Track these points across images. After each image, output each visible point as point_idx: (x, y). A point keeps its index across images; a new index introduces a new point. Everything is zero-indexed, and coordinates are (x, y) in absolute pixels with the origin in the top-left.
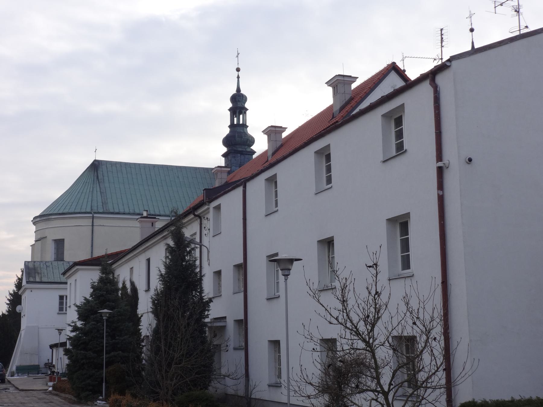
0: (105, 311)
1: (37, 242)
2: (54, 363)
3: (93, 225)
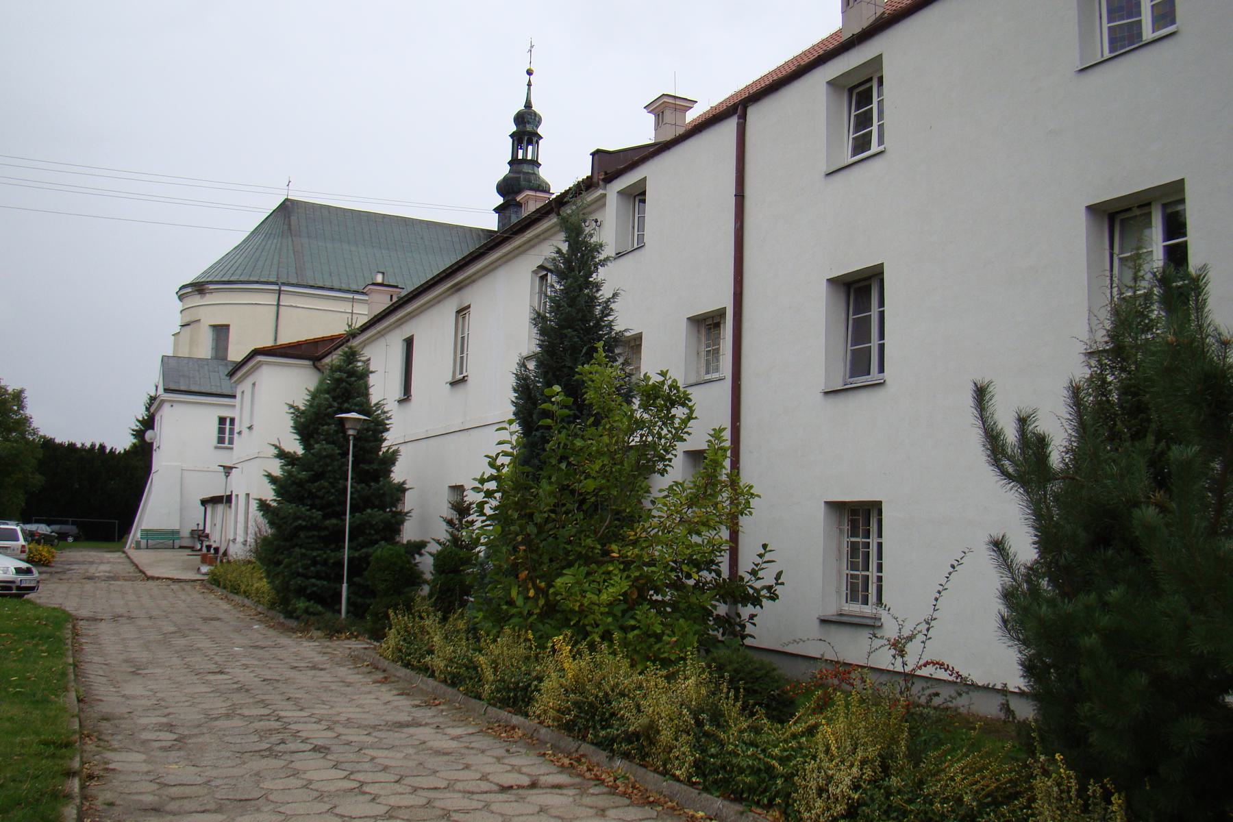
0: (354, 415)
1: (183, 328)
2: (207, 531)
3: (278, 305)
